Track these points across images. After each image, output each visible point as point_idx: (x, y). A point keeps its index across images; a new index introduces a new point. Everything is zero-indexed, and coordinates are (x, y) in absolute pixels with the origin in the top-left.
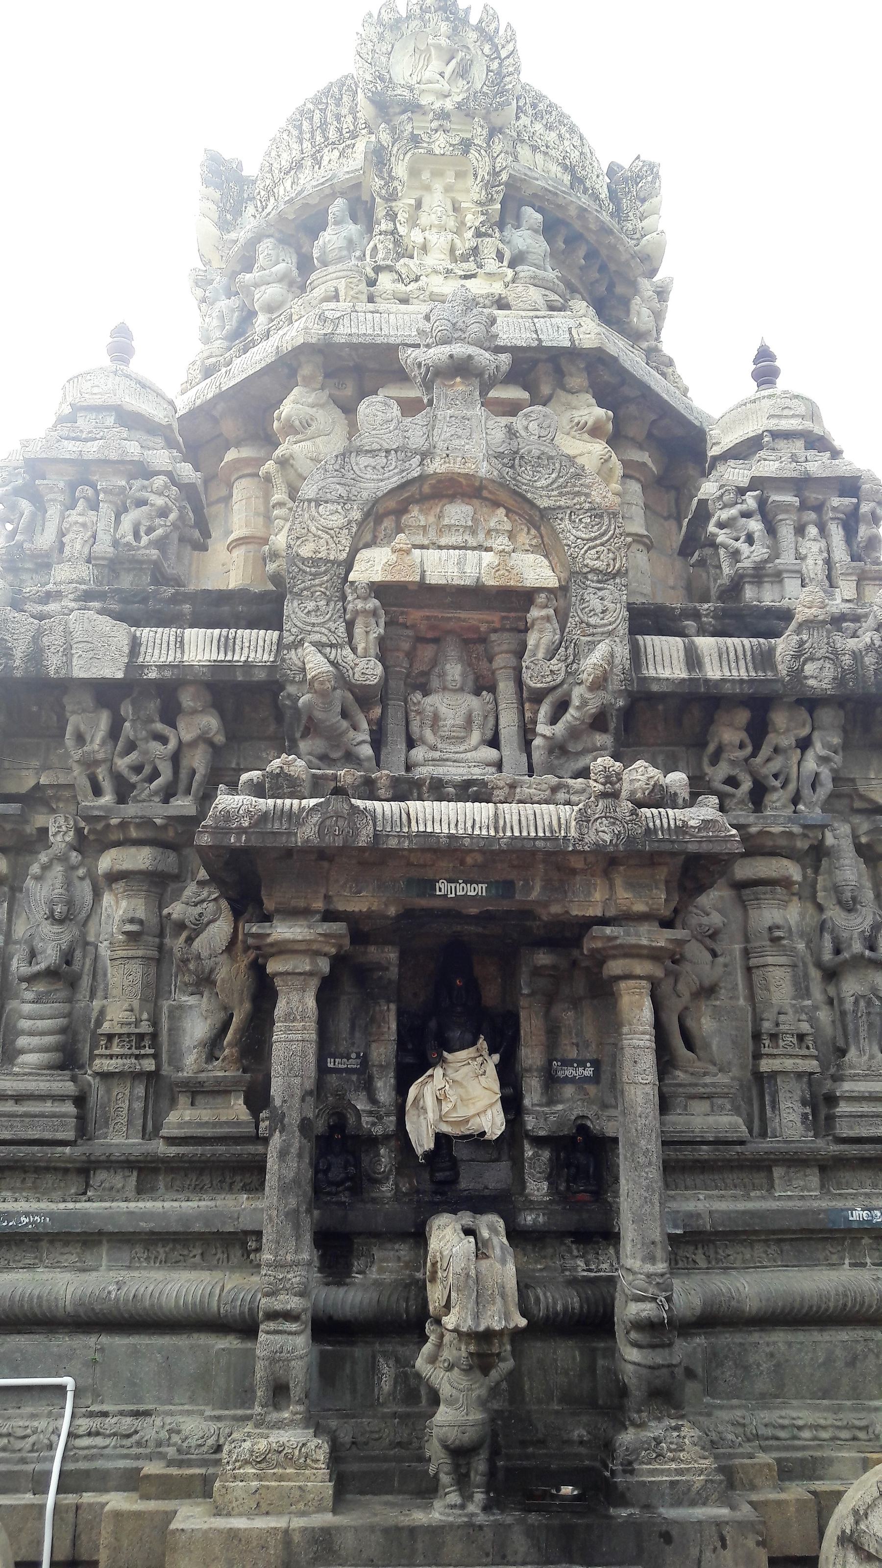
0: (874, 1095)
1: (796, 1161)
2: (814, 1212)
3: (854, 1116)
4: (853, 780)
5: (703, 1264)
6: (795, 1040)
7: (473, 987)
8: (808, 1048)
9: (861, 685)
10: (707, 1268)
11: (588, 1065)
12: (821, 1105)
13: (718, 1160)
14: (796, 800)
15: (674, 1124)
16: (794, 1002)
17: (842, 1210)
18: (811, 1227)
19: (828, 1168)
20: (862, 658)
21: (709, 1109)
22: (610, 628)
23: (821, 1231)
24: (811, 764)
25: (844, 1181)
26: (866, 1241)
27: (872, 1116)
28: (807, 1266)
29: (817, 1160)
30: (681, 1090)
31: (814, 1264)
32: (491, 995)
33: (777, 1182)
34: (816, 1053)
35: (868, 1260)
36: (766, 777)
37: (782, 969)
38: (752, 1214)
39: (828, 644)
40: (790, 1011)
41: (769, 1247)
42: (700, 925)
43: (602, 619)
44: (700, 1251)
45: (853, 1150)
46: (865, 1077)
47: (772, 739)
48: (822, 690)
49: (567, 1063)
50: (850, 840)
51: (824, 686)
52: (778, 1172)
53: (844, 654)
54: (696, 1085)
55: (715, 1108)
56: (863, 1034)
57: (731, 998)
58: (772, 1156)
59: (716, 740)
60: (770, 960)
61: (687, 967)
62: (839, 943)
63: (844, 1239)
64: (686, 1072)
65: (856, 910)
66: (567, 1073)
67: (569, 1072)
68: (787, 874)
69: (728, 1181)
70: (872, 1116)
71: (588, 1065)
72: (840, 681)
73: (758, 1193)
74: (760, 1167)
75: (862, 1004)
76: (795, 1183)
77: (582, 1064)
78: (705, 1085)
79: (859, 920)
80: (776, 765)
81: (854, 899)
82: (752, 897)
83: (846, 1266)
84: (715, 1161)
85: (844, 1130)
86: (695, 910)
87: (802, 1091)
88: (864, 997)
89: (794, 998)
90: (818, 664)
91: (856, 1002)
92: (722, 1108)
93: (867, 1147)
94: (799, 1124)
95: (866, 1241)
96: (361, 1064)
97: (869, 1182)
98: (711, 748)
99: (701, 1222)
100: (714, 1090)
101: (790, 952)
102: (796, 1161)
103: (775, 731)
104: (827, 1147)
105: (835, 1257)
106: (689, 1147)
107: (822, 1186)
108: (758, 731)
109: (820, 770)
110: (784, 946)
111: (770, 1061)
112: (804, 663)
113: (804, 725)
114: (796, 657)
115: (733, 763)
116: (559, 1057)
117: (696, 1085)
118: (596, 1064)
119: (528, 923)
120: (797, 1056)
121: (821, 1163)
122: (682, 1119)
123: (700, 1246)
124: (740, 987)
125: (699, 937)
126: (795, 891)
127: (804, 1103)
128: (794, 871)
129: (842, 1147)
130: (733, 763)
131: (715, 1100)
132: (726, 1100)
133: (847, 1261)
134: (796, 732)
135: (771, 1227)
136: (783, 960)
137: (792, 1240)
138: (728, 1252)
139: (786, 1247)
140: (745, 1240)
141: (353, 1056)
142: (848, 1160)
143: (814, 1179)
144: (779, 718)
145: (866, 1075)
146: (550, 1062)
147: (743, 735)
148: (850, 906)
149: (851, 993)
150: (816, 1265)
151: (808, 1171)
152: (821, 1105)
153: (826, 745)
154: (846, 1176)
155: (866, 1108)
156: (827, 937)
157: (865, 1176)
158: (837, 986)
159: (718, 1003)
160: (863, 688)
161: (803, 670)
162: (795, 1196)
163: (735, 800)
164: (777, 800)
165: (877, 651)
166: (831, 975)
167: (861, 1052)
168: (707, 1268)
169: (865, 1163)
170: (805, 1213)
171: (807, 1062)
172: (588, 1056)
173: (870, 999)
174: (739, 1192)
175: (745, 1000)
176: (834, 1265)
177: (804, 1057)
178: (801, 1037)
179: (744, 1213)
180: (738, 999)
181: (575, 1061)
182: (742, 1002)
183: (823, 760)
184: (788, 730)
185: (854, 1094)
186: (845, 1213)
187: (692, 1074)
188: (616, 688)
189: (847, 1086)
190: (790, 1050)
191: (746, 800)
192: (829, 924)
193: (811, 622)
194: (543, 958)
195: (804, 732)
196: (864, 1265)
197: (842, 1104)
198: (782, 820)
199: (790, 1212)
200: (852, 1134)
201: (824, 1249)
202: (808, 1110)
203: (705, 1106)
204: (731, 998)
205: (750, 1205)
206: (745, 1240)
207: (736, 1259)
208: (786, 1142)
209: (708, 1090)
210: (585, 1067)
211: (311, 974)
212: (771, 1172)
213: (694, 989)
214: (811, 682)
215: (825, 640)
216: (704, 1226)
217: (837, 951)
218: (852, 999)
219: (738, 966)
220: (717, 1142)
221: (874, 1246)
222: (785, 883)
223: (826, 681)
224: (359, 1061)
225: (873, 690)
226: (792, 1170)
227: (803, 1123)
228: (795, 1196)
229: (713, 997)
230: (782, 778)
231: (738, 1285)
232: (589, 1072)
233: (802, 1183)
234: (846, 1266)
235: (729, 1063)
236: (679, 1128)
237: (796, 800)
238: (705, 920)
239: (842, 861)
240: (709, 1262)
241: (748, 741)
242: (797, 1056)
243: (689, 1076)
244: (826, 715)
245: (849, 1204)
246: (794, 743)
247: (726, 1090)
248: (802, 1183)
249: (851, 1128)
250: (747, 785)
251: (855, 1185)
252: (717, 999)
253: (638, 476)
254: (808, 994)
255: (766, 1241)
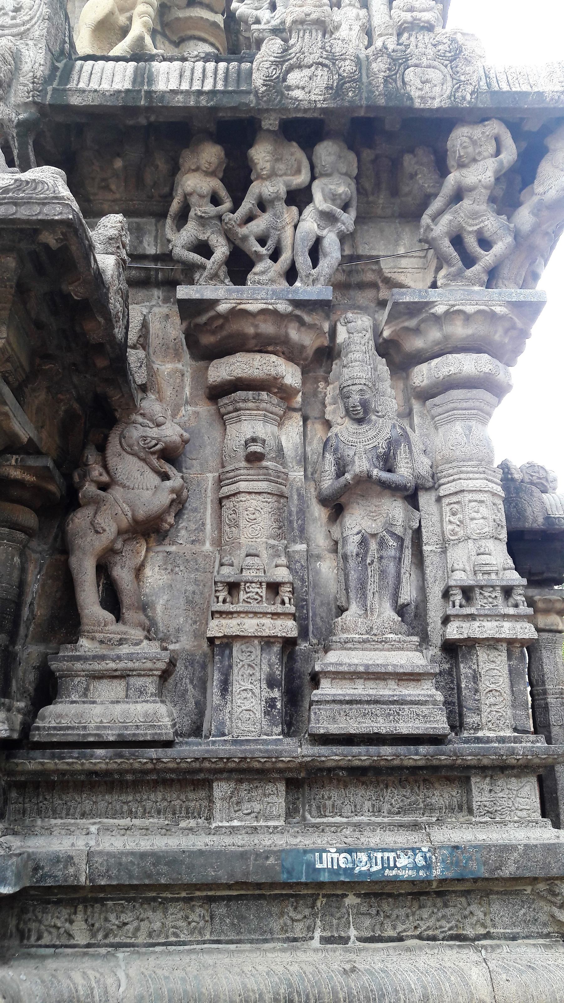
0: (371, 670)
1: (249, 772)
2: (258, 855)
3: (341, 702)
4: (375, 260)
5: (81, 939)
6: (263, 592)
8: (283, 603)
9: (364, 95)
10: (88, 946)
12: (294, 688)
13: (127, 771)
14: (291, 275)
15: (60, 716)
16: (272, 542)
17: (305, 852)
18: (252, 879)
19: (302, 783)
20: (369, 64)
21: (122, 694)
22: (22, 29)
23: (273, 885)
24: (310, 223)
25: (329, 803)
26: (351, 900)
27: (368, 702)
28: (251, 942)
29: (280, 771)
30: (78, 665)
31: (264, 937)
33: (218, 804)
34: (293, 609)
35: (353, 933)
36: (245, 238)
37: (260, 498)
38: (157, 858)
39: (323, 48)
40: (264, 554)
41: (192, 909)
42: (144, 438)
43: (14, 18)
44: (80, 917)
45: (334, 755)
46: (364, 644)
47: (257, 189)
48: (310, 102)
50: (369, 335)
51: (313, 98)
52: (221, 789)
53: (345, 60)
54: (103, 658)
55: (131, 692)
56: (372, 587)
57: (193, 542)
58: (207, 765)
59: (180, 191)
60: (243, 486)
61: (117, 492)
63: (315, 897)
64: (93, 639)
65: (370, 421)
68: (273, 373)
69: (149, 804)
70: (368, 702)
72: (336, 90)
73: (192, 823)
74: (188, 781)
75: (373, 545)
76: (246, 807)
78: (119, 658)
79: (371, 433)
80: (260, 224)
81: (365, 405)
82: (231, 408)
83: (316, 943)
84: (122, 772)
85: (323, 722)
86: (140, 419)
87: (270, 666)
88: (374, 535)
89: (278, 537)
90: (307, 72)
91: (364, 543)
92: (141, 692)
93: (355, 750)
94: (258, 715)
95: (351, 900)
97: (368, 805)
98: (175, 206)
99: (71, 870)
100: (130, 665)
101: (280, 478)
102: (249, 772)
103: (259, 177)
104: (299, 751)
105: (299, 926)
106: (76, 752)
107: (290, 813)
108: (237, 178)
109: (325, 232)
110: (266, 468)
111: (224, 622)
112: (288, 72)
113: (298, 171)
114: (278, 64)
115: (203, 221)
117: (103, 658)
120: (265, 614)
121: (290, 775)
122: (73, 709)
123: (80, 907)
124: (208, 527)
125: (142, 454)
126: (298, 406)
127: (271, 683)
128: (291, 375)
129: (323, 750)
130: (203, 221)
131: (132, 680)
132: (150, 680)
133: (317, 934)
134: (286, 178)
135: (186, 879)
136: (263, 486)
137: (229, 898)
138: (124, 918)
139: (221, 910)
140: (154, 899)
142: (330, 770)
143: (276, 799)
144: (261, 154)
145: (364, 641)
147: (215, 184)
148: (360, 415)
149: (356, 530)
150: (266, 941)
151: (270, 788)
152: (294, 688)
153: (333, 198)
154: (333, 795)
155: (360, 689)
156: (329, 457)
157: (362, 796)
158: (342, 526)
159: (173, 549)
160: (368, 99)
161: (284, 80)
162: (245, 829)
163: (206, 273)
164: (265, 271)
165: (389, 56)
166: (336, 507)
167: (366, 610)
168: (88, 946)
169: (359, 775)
170: (243, 856)
171: (279, 622)
173: (382, 538)
174: (162, 821)
175: (212, 544)
176: (295, 940)
177: (276, 615)
178: (274, 588)
179: (143, 855)
180: (204, 543)
182: (208, 547)
183: (328, 218)
184: (273, 175)
185: (341, 669)
186: (309, 857)
187: (101, 642)
188: (20, 100)
189: (333, 657)
190: (254, 606)
191: (221, 274)
192: (333, 441)
193: (302, 22)
195: (302, 179)
196: (345, 940)
197: (325, 683)
198: (263, 294)
199: (218, 854)
200: (334, 729)
201: (282, 914)
202: (276, 694)
203: (117, 688)
204: (193, 542)
205: (145, 844)
206: (154, 899)
207: (137, 929)
208: (235, 742)
209: (121, 665)
212: (211, 788)
213: (125, 524)
214: (297, 94)
215: (320, 44)
216: (76, 877)
217: (340, 473)
218: (358, 538)
219: (209, 500)
220: (122, 743)
221: (364, 909)
222: (284, 393)
223: (317, 91)
225: (382, 101)
226: (245, 786)
227: (267, 713)
228: (245, 829)
229: (167, 541)
230: (271, 243)
231: (110, 981)
233: (257, 807)
234: (316, 943)
235: (178, 630)
236: (64, 722)
237: (291, 275)
238: (154, 432)
239: (350, 355)
240: (94, 935)
241: (223, 193)
242: (265, 614)
243: (97, 645)
244: (326, 152)
245: (319, 841)
246: (284, 196)
247: (149, 665)
248: (257, 807)
249: (334, 720)
250: (221, 251)
251: (347, 809)
252: (174, 543)
253: (212, 40)
254: (303, 535)
255: (188, 900)
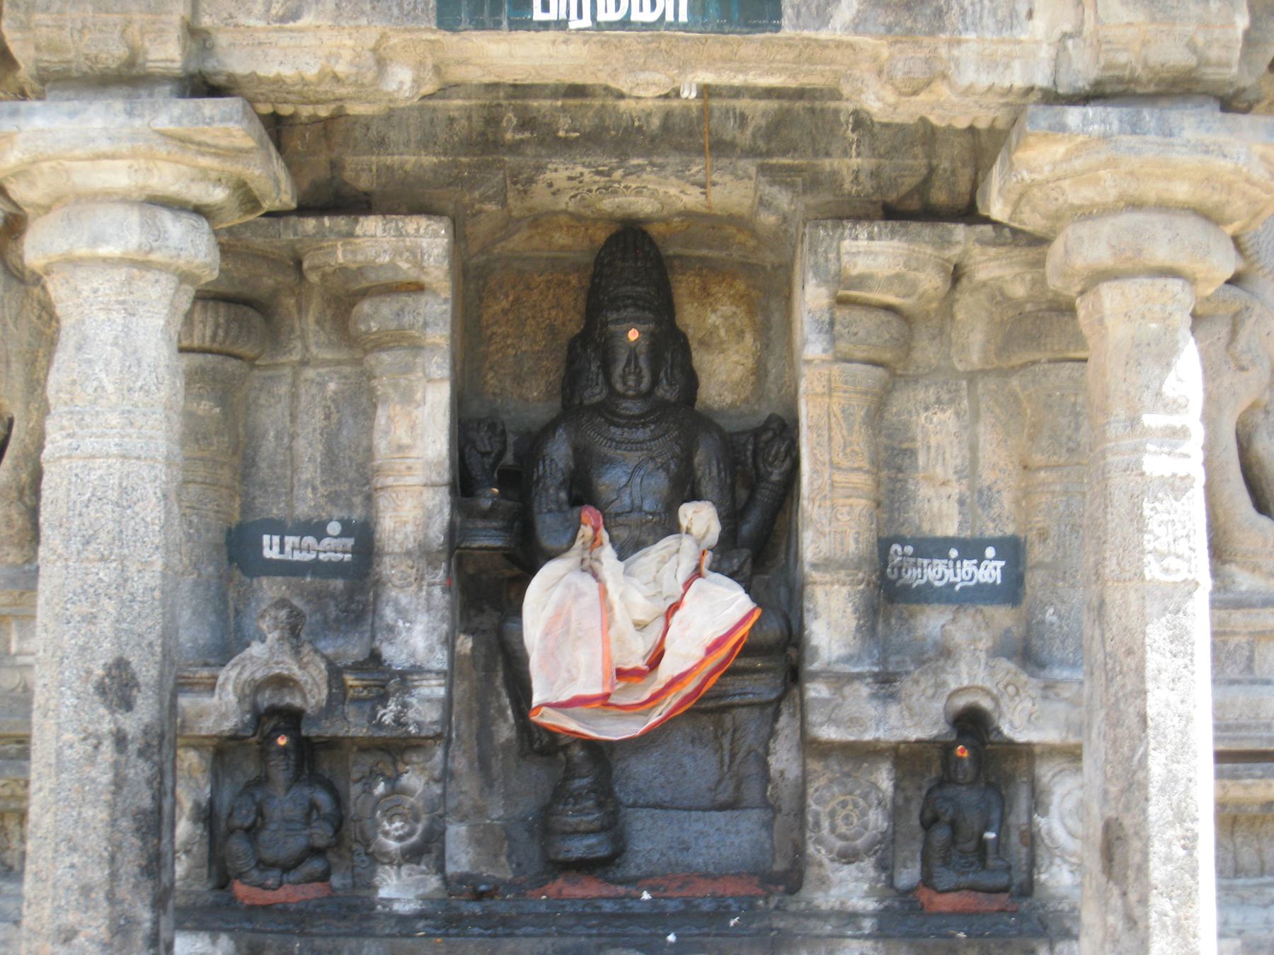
7: (672, 348)
11: (990, 552)
32: (723, 376)
49: (933, 548)
62: (907, 600)
66: (930, 574)
67: (936, 572)
71: (990, 552)
77: (972, 549)
96: (354, 551)
116: (906, 531)
118: (1012, 550)
119: (826, 164)
141: (334, 528)
146: (884, 545)
172: (991, 531)
181: (949, 542)
194: (874, 254)
210: (981, 558)
211: (141, 264)
224: (350, 542)
232: (991, 571)
